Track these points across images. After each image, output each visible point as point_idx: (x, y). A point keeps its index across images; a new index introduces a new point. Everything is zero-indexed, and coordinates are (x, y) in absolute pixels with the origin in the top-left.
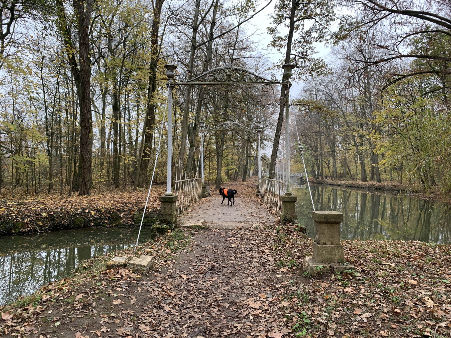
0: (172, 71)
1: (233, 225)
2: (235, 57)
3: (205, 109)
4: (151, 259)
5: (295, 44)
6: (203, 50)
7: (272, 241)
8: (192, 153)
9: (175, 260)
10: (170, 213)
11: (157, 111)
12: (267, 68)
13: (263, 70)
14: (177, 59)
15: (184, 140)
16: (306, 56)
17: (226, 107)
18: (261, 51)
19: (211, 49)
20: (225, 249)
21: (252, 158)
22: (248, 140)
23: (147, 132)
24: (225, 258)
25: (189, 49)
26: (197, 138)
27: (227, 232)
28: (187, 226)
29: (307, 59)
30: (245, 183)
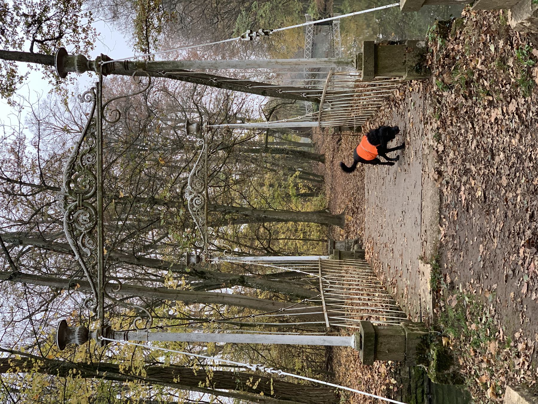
0: (71, 332)
1: (430, 191)
2: (37, 181)
3: (156, 248)
4: (512, 391)
5: (7, 41)
6: (21, 254)
7: (470, 102)
8: (258, 280)
9: (515, 332)
10: (401, 340)
11: (161, 359)
12: (63, 108)
13: (67, 115)
14: (43, 313)
15: (230, 300)
16: (34, 16)
17: (154, 201)
18: (23, 121)
19: (19, 233)
20: (488, 213)
21: (270, 139)
22: (228, 149)
23: (211, 384)
24: (509, 214)
25: (19, 285)
26: (224, 270)
27: (448, 206)
28: (434, 300)
29: (41, 14)
30: (328, 156)
